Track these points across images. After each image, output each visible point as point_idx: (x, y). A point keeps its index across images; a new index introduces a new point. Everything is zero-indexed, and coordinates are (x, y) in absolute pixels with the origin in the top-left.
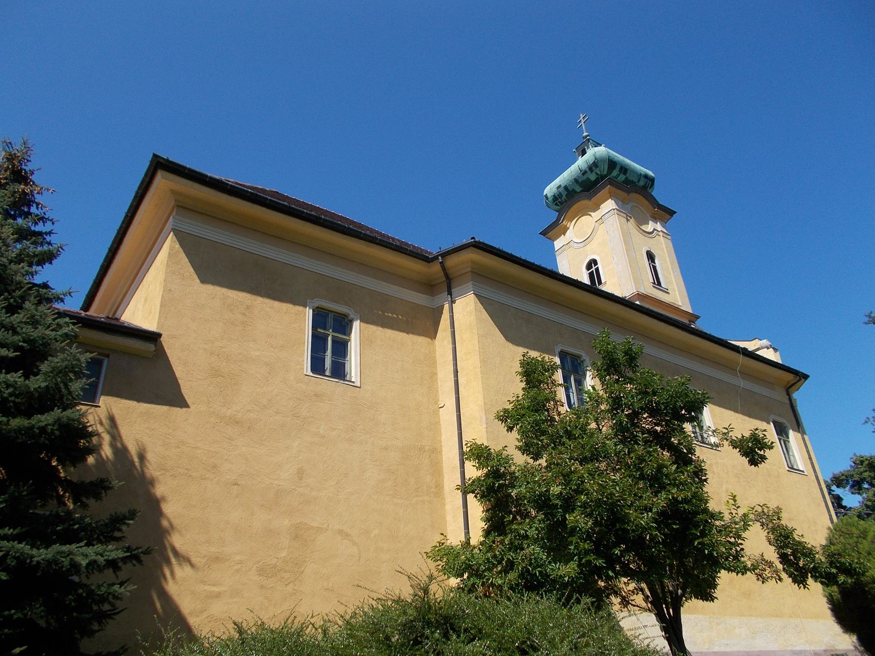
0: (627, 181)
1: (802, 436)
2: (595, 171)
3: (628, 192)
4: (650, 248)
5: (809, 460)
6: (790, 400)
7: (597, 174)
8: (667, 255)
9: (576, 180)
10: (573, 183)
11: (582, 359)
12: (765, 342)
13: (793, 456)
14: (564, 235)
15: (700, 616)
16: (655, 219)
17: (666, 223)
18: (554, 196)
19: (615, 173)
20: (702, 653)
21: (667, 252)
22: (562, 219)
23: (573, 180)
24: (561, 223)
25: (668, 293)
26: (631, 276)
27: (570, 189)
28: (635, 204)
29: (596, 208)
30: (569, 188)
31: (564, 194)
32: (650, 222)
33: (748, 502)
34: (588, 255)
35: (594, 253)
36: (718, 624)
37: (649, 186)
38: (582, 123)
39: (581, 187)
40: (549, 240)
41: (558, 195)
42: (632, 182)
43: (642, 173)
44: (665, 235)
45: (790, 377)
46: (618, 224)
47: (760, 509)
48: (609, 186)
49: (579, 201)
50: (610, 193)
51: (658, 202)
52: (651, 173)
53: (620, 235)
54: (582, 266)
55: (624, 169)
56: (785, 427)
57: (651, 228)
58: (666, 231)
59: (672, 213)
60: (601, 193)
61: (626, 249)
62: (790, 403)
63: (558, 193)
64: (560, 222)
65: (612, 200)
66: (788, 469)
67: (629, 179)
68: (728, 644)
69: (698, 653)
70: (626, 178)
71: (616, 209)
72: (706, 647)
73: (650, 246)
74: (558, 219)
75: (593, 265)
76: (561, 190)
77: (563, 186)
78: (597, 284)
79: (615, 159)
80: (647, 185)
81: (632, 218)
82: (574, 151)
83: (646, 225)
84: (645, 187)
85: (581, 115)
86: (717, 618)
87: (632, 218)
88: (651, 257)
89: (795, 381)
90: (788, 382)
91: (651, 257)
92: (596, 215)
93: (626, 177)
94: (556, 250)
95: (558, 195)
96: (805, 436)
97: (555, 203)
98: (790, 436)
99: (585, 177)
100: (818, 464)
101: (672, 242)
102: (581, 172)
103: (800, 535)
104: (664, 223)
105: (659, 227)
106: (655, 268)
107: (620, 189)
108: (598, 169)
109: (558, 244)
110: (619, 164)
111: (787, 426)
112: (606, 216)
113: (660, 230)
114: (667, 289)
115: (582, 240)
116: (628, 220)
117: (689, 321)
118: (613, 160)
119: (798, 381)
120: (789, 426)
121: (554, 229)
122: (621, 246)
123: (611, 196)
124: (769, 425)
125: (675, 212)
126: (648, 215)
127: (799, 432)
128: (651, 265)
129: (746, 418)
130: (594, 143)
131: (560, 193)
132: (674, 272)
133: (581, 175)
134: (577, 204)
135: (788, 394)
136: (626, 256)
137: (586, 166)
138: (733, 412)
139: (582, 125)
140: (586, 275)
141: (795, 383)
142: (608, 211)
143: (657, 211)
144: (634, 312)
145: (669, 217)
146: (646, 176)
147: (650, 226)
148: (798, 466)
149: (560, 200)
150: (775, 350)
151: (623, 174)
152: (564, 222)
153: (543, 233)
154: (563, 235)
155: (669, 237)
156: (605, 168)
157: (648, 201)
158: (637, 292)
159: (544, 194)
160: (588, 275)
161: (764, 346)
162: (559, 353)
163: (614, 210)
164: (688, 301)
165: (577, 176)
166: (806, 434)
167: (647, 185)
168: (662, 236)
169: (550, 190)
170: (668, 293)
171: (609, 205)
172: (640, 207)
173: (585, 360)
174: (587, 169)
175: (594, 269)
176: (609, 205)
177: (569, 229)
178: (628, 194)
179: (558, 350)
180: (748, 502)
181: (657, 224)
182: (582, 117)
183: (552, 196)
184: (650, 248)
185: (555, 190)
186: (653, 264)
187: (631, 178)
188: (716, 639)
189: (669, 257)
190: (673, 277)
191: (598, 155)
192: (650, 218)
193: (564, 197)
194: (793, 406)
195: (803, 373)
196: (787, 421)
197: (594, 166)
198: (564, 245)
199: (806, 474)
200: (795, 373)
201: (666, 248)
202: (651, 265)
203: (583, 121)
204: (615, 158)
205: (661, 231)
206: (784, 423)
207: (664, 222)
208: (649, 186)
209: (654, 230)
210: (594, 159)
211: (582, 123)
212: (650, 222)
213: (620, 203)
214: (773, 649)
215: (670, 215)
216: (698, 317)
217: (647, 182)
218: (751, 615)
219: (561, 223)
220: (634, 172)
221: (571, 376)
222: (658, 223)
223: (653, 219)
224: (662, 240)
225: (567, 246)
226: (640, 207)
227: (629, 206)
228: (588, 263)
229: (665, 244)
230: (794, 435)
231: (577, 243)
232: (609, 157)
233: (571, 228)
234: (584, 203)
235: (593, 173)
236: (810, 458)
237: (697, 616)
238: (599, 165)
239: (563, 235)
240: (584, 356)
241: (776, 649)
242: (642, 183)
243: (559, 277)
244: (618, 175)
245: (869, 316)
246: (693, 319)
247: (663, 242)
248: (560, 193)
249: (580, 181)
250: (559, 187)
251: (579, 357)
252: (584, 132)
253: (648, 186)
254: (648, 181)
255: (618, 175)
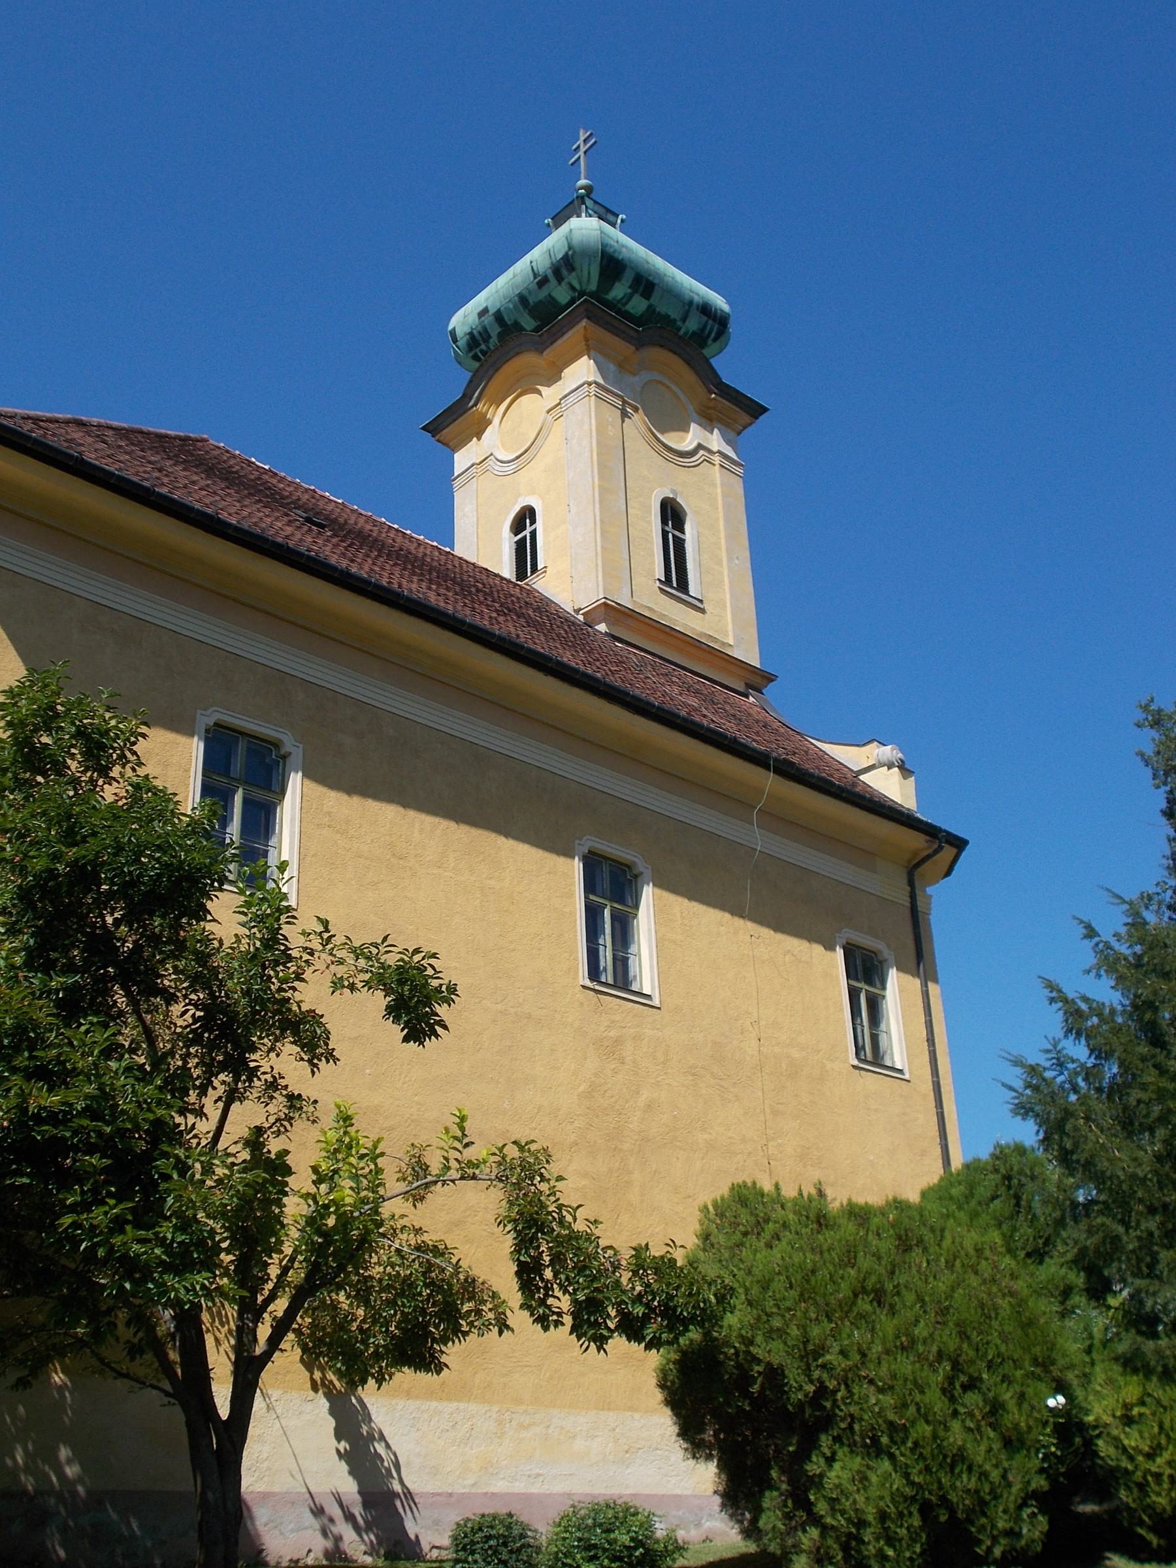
0: (651, 319)
1: (925, 986)
2: (566, 280)
3: (639, 343)
4: (673, 491)
5: (926, 1043)
6: (913, 896)
7: (573, 288)
8: (721, 515)
9: (523, 299)
10: (515, 306)
11: (282, 752)
12: (888, 752)
13: (888, 1033)
14: (479, 439)
15: (473, 1407)
16: (709, 420)
17: (739, 433)
18: (471, 334)
19: (619, 291)
20: (451, 1495)
21: (724, 505)
22: (476, 395)
23: (516, 298)
24: (472, 407)
25: (703, 611)
26: (600, 558)
27: (509, 323)
28: (657, 376)
29: (553, 377)
30: (506, 318)
31: (495, 331)
32: (693, 426)
33: (706, 1136)
34: (520, 495)
35: (532, 492)
36: (522, 1427)
37: (713, 335)
38: (581, 153)
39: (534, 318)
40: (445, 448)
41: (480, 333)
42: (667, 320)
43: (696, 299)
44: (727, 464)
45: (917, 841)
46: (593, 421)
47: (512, 1152)
48: (584, 322)
49: (518, 354)
50: (587, 340)
51: (720, 379)
52: (719, 302)
53: (592, 451)
54: (503, 523)
55: (646, 284)
56: (881, 962)
57: (690, 443)
58: (735, 457)
59: (756, 410)
60: (566, 337)
61: (600, 487)
62: (911, 903)
63: (479, 328)
64: (471, 404)
65: (590, 358)
66: (856, 1062)
67: (658, 310)
68: (539, 1475)
69: (438, 1494)
70: (651, 309)
71: (596, 383)
72: (470, 1481)
73: (679, 489)
74: (466, 396)
75: (528, 521)
76: (488, 320)
77: (492, 311)
78: (529, 570)
79: (620, 253)
80: (707, 332)
81: (641, 411)
82: (548, 225)
83: (681, 434)
84: (700, 339)
85: (581, 134)
86: (525, 1412)
87: (641, 411)
88: (672, 514)
89: (930, 851)
90: (916, 853)
91: (672, 514)
92: (550, 394)
93: (650, 306)
94: (456, 474)
95: (480, 333)
96: (930, 985)
97: (471, 354)
98: (889, 985)
99: (542, 294)
100: (952, 1053)
101: (744, 482)
102: (535, 278)
103: (592, 1220)
104: (732, 435)
105: (715, 440)
106: (680, 545)
107: (617, 335)
108: (574, 274)
109: (462, 459)
110: (632, 269)
111: (886, 960)
112: (571, 398)
113: (715, 449)
114: (701, 601)
115: (513, 457)
116: (624, 415)
117: (746, 684)
118: (616, 255)
119: (936, 852)
120: (891, 959)
121: (455, 420)
122: (590, 479)
123: (590, 348)
124: (829, 953)
125: (765, 410)
126: (691, 408)
127: (918, 976)
128: (670, 536)
129: (766, 932)
130: (596, 208)
131: (485, 329)
132: (730, 560)
133: (534, 286)
134: (514, 360)
135: (911, 883)
136: (597, 506)
137: (547, 263)
138: (727, 916)
139: (579, 158)
140: (507, 545)
141: (929, 857)
142: (574, 386)
143: (714, 399)
144: (448, 634)
145: (746, 418)
146: (706, 309)
147: (692, 437)
148: (893, 1062)
149: (483, 347)
150: (905, 770)
151: (642, 295)
152: (480, 406)
153: (431, 428)
154: (475, 439)
155: (740, 471)
156: (590, 276)
157: (697, 374)
158: (603, 600)
159: (450, 327)
160: (514, 546)
161: (884, 759)
162: (207, 731)
163: (590, 384)
164: (756, 635)
165: (526, 288)
166: (936, 981)
167: (707, 332)
168: (717, 467)
169: (463, 319)
170: (703, 611)
171: (583, 370)
172: (673, 387)
173: (290, 754)
174: (550, 273)
175: (527, 533)
176: (583, 370)
177: (490, 423)
178: (637, 349)
179: (207, 719)
180: (706, 1136)
181: (712, 433)
182: (582, 138)
183: (466, 334)
184: (673, 491)
185: (473, 320)
186: (677, 533)
187: (662, 309)
188: (505, 1463)
189: (727, 520)
190: (726, 572)
191: (577, 238)
192: (695, 414)
193: (494, 340)
194: (917, 911)
195: (949, 833)
196: (889, 946)
197: (565, 265)
198: (472, 465)
199: (907, 1077)
200: (930, 831)
201: (724, 495)
202: (670, 536)
203: (583, 149)
204: (624, 250)
205: (719, 452)
206: (881, 952)
207: (733, 433)
208: (713, 335)
209: (700, 446)
210: (567, 248)
211: (581, 153)
212: (693, 426)
213: (612, 367)
214: (678, 1491)
215: (752, 416)
216: (770, 678)
217: (706, 323)
218: (632, 1409)
219: (472, 407)
220: (673, 293)
221: (234, 792)
222: (716, 431)
223: (702, 420)
224: (718, 475)
225: (480, 469)
226: (673, 387)
227: (637, 381)
228: (514, 518)
229: (722, 485)
230: (898, 977)
231: (502, 462)
232: (604, 246)
233: (496, 421)
234: (527, 360)
235: (563, 284)
236: (931, 1040)
237: (462, 1405)
238: (577, 265)
239: (475, 439)
240: (289, 742)
241: (689, 1492)
242: (693, 324)
243: (229, 531)
244: (629, 298)
245: (1145, 708)
246: (757, 680)
247: (718, 482)
248: (485, 329)
249: (531, 301)
250: (484, 312)
251: (277, 745)
252: (582, 175)
253: (709, 336)
254: (710, 322)
255: (629, 298)
